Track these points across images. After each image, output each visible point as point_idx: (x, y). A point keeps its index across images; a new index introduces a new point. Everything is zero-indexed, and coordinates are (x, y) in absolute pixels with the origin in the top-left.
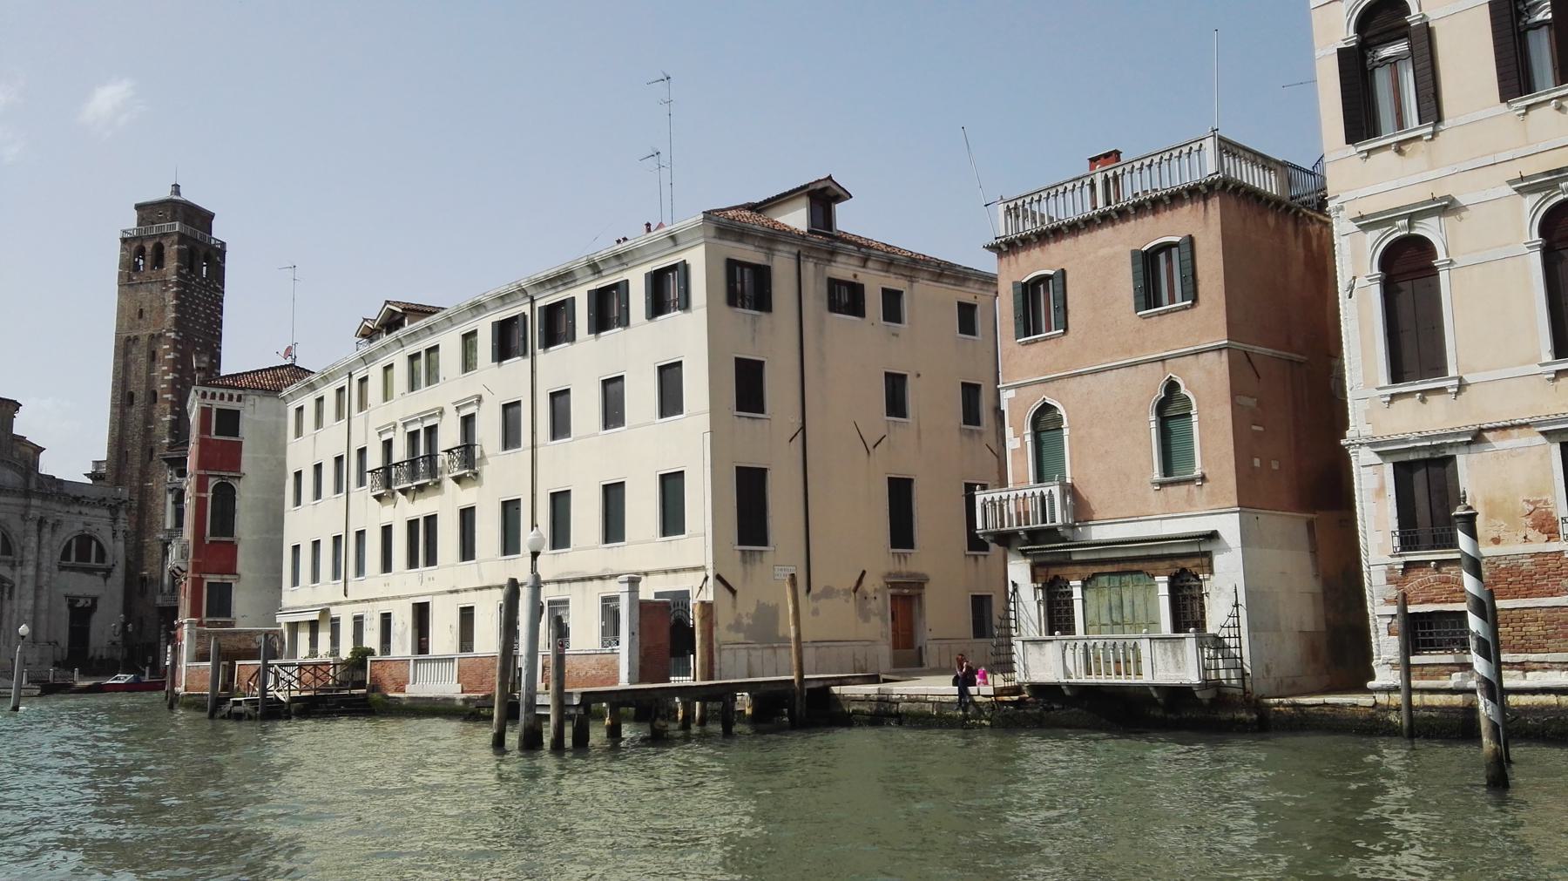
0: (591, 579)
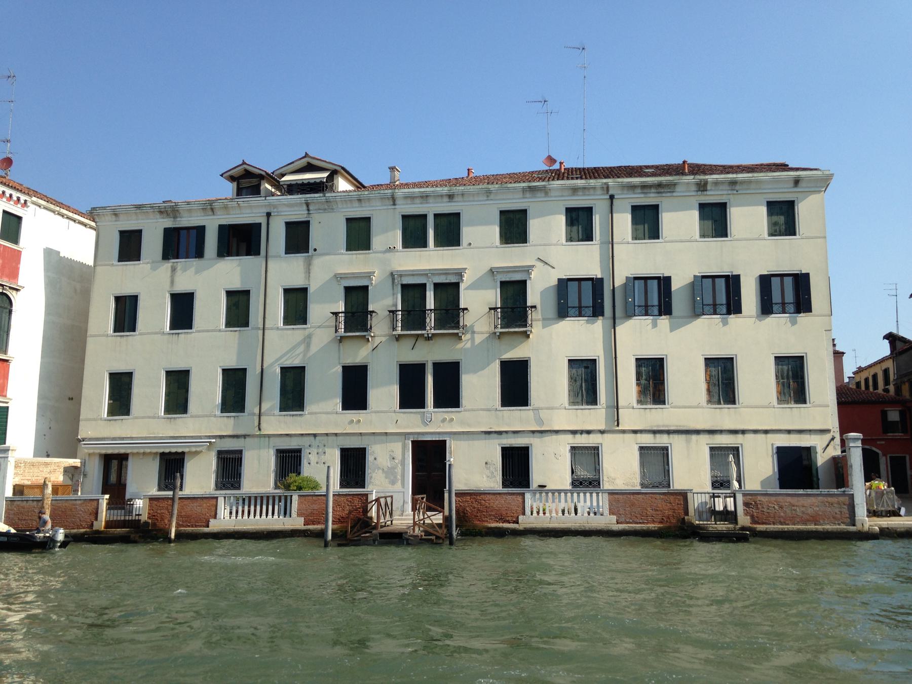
0: (698, 432)
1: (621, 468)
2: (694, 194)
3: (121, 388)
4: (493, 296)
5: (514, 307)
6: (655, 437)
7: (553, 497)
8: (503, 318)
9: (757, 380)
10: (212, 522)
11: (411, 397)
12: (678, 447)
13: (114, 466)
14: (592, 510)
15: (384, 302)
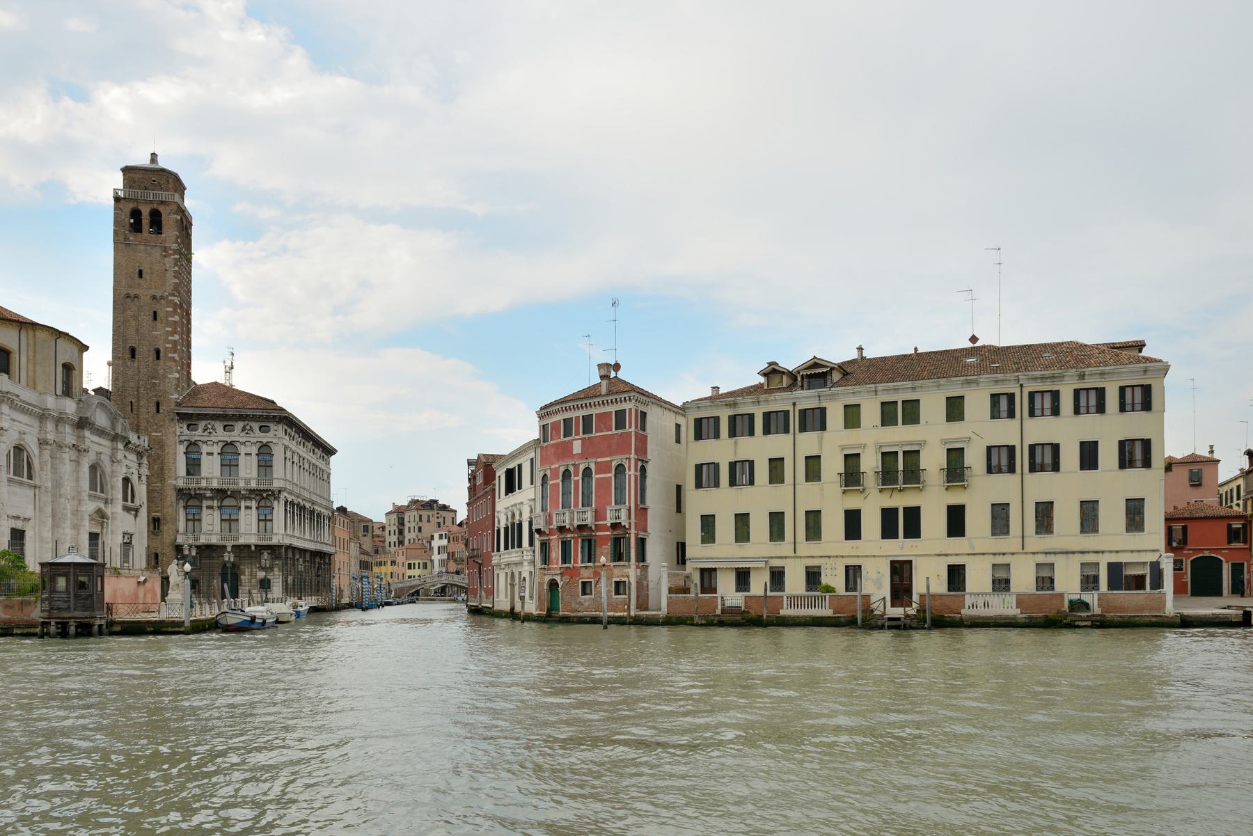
0: (1073, 553)
1: (1023, 579)
3: (708, 523)
4: (943, 461)
5: (955, 470)
7: (978, 593)
8: (948, 476)
11: (889, 531)
12: (1059, 562)
13: (708, 575)
14: (1004, 606)
15: (870, 464)
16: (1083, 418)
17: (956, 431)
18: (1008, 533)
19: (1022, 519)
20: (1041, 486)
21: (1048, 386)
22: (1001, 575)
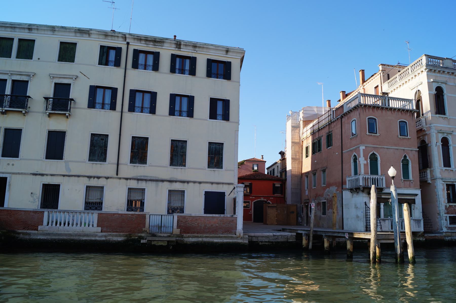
0: (163, 181)
1: (115, 200)
2: (173, 49)
6: (138, 183)
9: (197, 155)
10: (40, 228)
12: (149, 188)
14: (88, 226)
16: (177, 76)
17: (66, 69)
18: (104, 160)
19: (119, 149)
20: (139, 124)
21: (151, 48)
22: (94, 198)
